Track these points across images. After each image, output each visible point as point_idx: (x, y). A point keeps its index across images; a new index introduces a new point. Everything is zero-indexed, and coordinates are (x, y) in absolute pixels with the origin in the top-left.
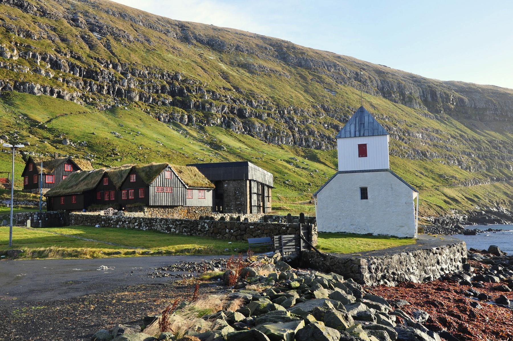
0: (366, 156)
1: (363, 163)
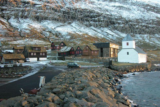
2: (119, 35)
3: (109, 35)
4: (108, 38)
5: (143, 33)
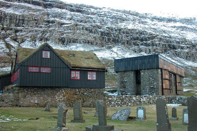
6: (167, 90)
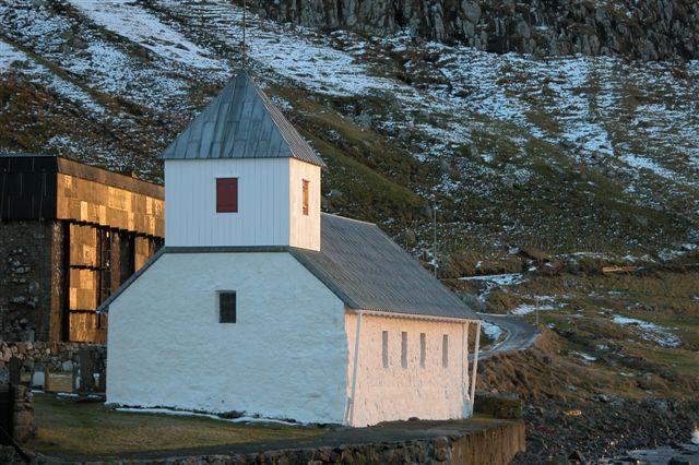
0: (236, 211)
1: (228, 230)
2: (222, 51)
3: (97, 48)
4: (80, 80)
5: (542, 42)
6: (85, 316)
